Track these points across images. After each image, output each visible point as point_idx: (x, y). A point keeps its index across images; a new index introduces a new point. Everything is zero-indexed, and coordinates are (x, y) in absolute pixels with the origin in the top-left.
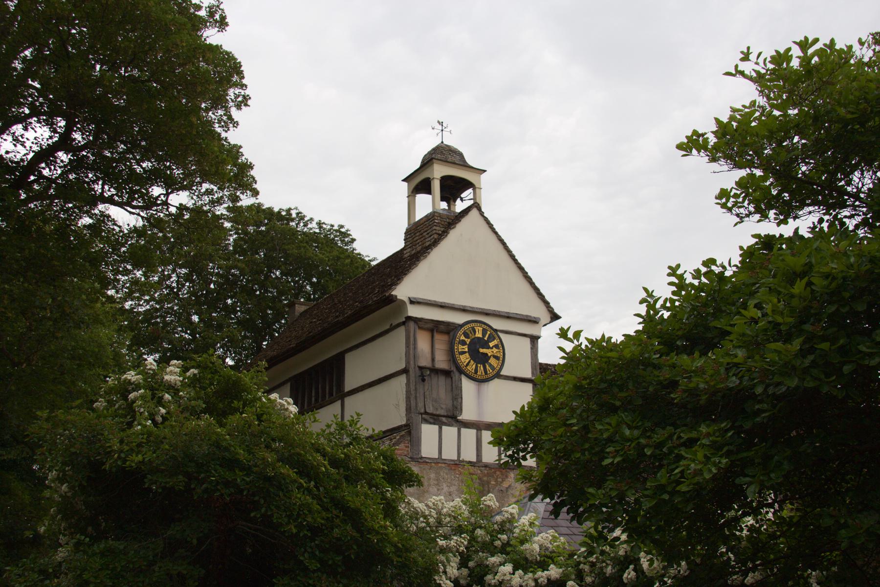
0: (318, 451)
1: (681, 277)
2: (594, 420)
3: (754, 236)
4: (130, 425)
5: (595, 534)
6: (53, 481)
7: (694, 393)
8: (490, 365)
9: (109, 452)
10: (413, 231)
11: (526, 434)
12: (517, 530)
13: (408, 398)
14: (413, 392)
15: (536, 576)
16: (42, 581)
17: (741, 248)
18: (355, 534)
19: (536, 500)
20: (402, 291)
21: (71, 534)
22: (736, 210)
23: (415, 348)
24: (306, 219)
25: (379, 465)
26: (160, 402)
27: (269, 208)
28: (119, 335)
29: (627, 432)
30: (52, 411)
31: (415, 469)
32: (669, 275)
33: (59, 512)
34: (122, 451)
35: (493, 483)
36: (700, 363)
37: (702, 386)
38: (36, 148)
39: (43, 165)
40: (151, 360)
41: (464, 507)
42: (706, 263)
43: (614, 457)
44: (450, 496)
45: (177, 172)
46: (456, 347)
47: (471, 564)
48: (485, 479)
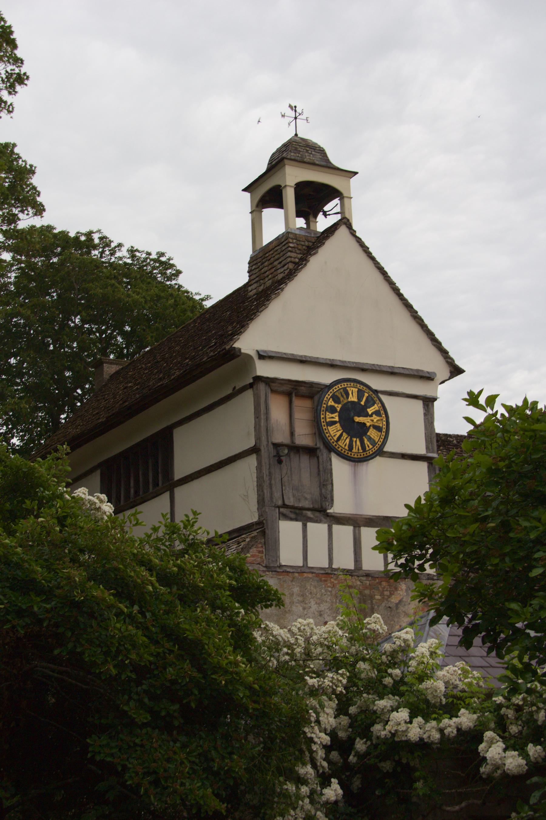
0: (142, 563)
8: (370, 439)
10: (259, 260)
12: (413, 663)
14: (266, 478)
15: (441, 725)
18: (195, 674)
23: (267, 419)
24: (113, 245)
31: (273, 582)
35: (378, 597)
41: (340, 633)
46: (322, 416)
47: (352, 710)
48: (367, 592)
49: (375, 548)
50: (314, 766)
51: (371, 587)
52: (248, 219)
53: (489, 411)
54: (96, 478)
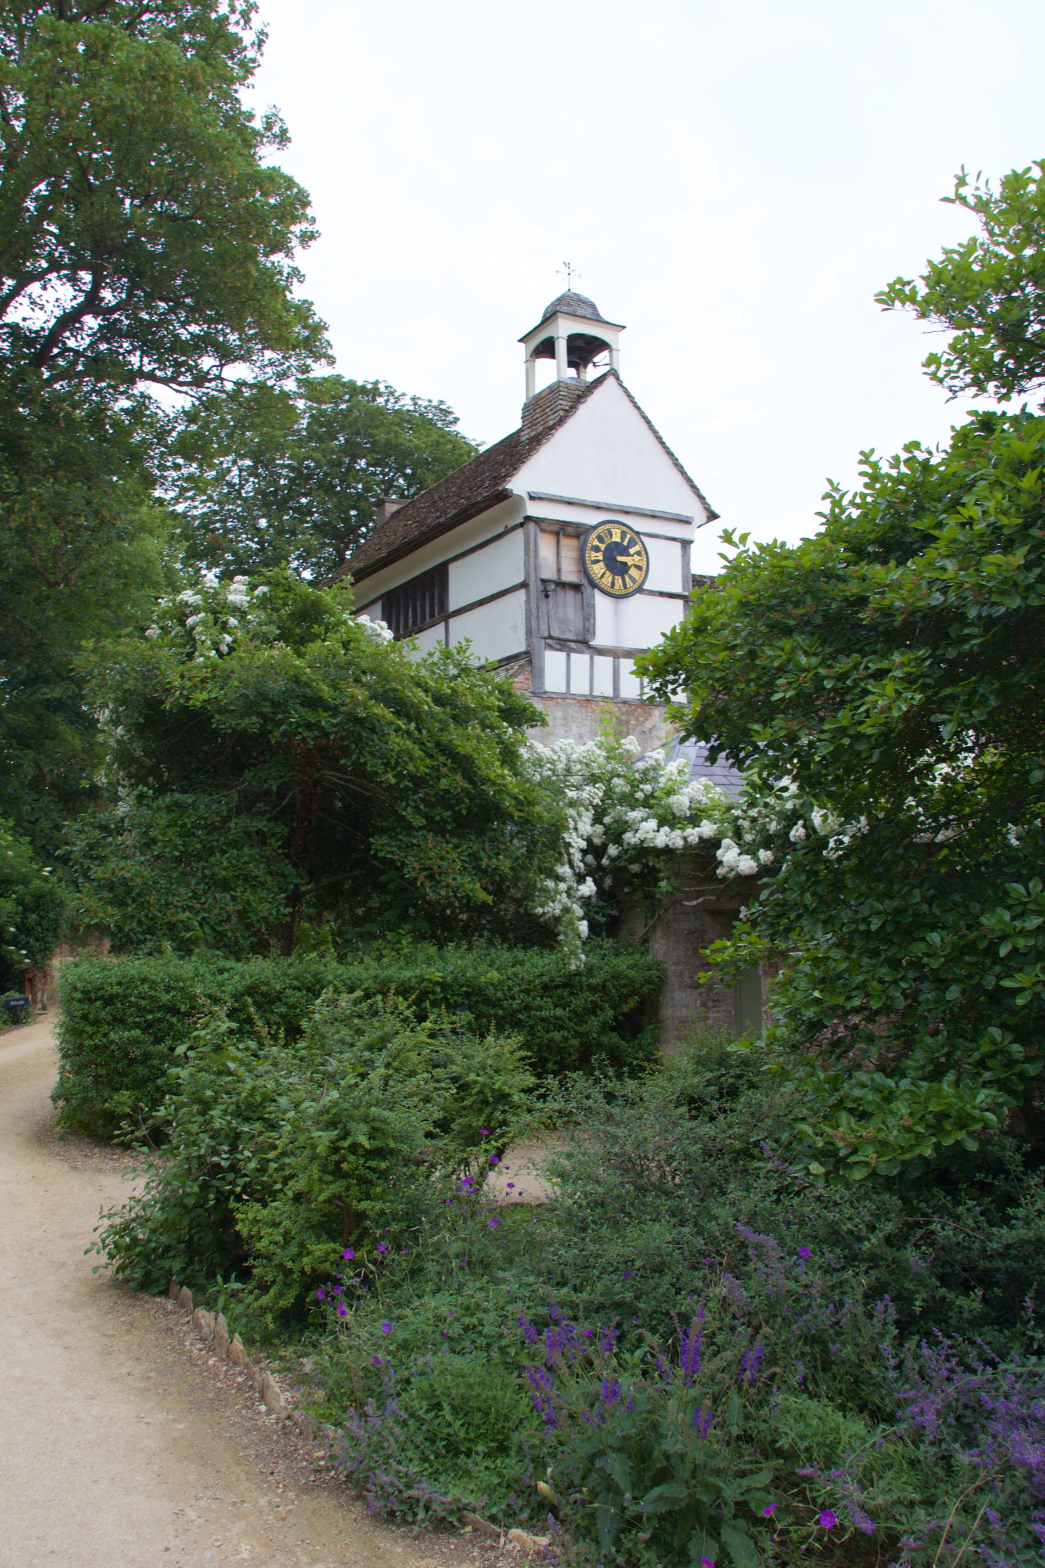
0: (418, 685)
1: (875, 466)
2: (763, 645)
3: (970, 413)
4: (190, 656)
5: (759, 782)
6: (106, 724)
7: (887, 612)
8: (631, 577)
9: (168, 690)
11: (678, 662)
12: (662, 780)
13: (528, 619)
14: (534, 611)
15: (685, 834)
16: (104, 838)
17: (953, 428)
18: (466, 785)
19: (687, 743)
20: (519, 484)
21: (132, 785)
22: (948, 382)
23: (536, 556)
24: (397, 394)
25: (494, 701)
26: (224, 628)
27: (350, 381)
28: (171, 546)
29: (803, 660)
30: (98, 641)
31: (538, 706)
32: (861, 462)
33: (116, 759)
34: (183, 688)
36: (896, 574)
37: (898, 604)
38: (59, 313)
39: (68, 334)
40: (210, 577)
41: (598, 752)
42: (907, 448)
43: (785, 691)
44: (581, 739)
45: (233, 338)
47: (607, 820)
48: (624, 717)
49: (632, 673)
50: (572, 866)
51: (627, 713)
52: (523, 367)
53: (742, 548)
54: (378, 608)
